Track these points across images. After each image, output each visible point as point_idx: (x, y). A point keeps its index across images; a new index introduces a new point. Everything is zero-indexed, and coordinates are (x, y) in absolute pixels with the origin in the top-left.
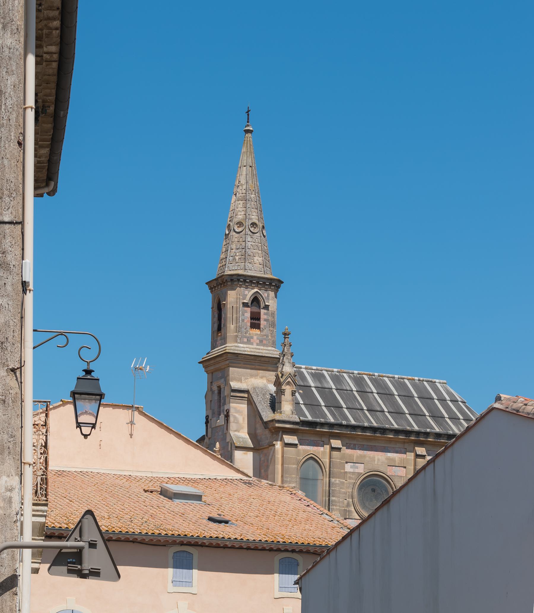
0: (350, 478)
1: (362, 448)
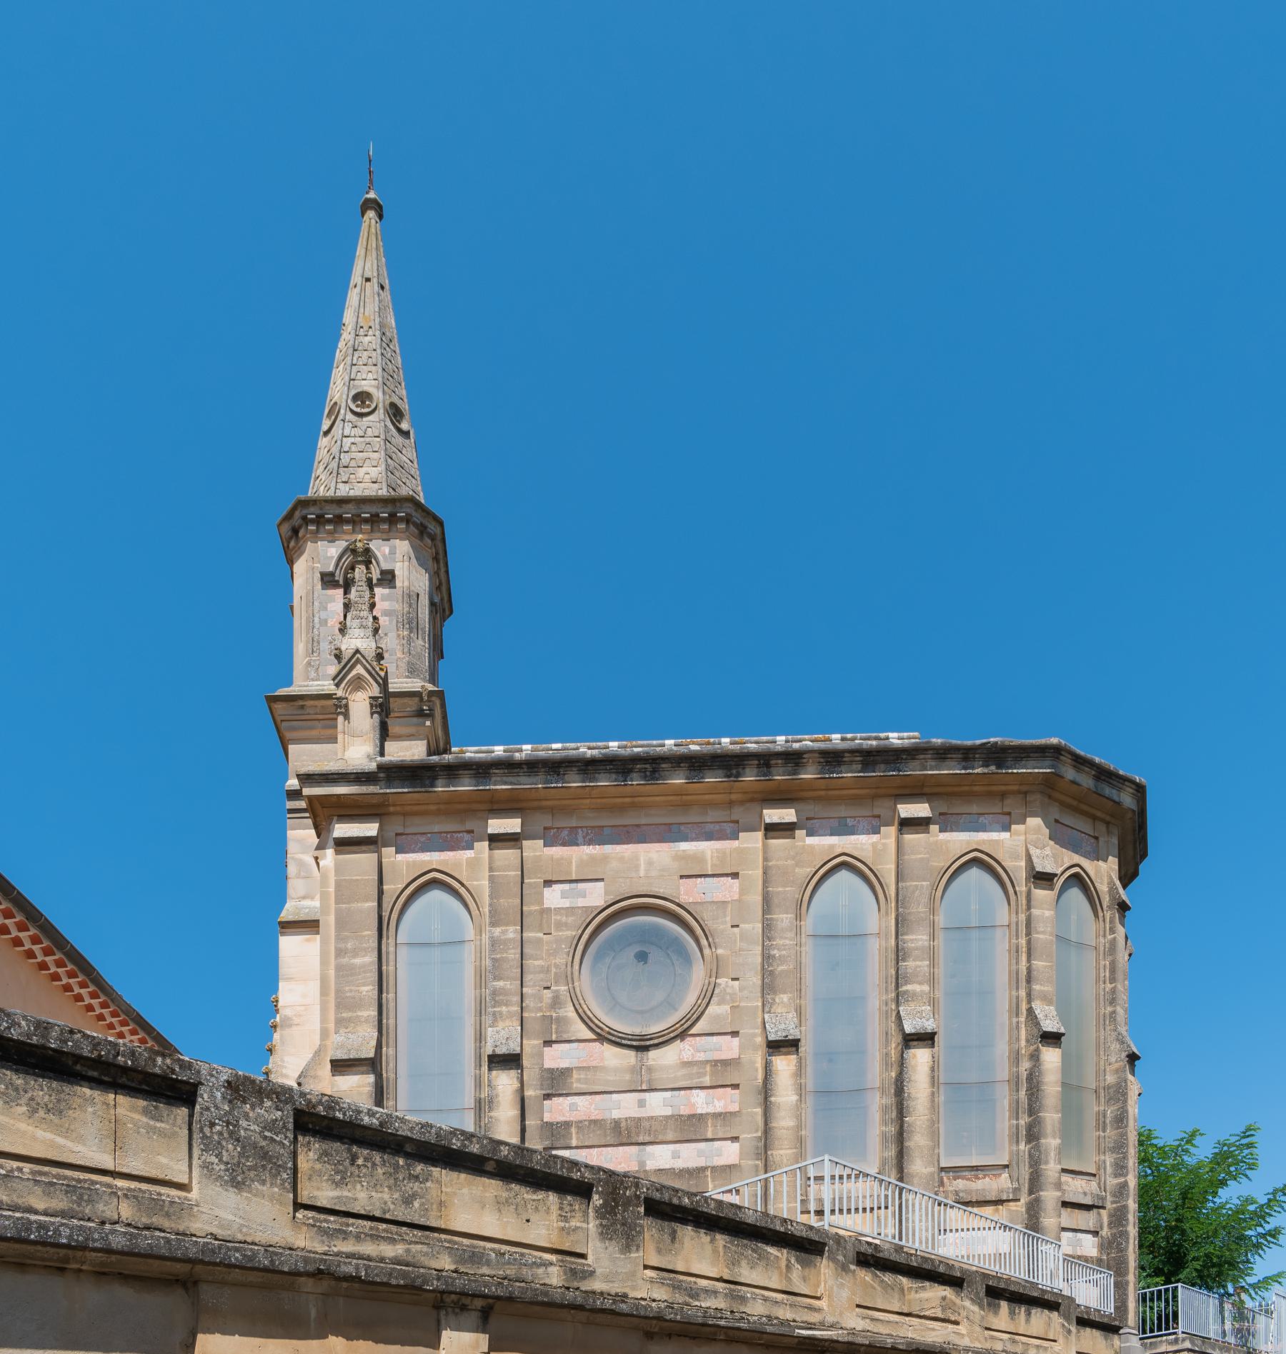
0: (559, 925)
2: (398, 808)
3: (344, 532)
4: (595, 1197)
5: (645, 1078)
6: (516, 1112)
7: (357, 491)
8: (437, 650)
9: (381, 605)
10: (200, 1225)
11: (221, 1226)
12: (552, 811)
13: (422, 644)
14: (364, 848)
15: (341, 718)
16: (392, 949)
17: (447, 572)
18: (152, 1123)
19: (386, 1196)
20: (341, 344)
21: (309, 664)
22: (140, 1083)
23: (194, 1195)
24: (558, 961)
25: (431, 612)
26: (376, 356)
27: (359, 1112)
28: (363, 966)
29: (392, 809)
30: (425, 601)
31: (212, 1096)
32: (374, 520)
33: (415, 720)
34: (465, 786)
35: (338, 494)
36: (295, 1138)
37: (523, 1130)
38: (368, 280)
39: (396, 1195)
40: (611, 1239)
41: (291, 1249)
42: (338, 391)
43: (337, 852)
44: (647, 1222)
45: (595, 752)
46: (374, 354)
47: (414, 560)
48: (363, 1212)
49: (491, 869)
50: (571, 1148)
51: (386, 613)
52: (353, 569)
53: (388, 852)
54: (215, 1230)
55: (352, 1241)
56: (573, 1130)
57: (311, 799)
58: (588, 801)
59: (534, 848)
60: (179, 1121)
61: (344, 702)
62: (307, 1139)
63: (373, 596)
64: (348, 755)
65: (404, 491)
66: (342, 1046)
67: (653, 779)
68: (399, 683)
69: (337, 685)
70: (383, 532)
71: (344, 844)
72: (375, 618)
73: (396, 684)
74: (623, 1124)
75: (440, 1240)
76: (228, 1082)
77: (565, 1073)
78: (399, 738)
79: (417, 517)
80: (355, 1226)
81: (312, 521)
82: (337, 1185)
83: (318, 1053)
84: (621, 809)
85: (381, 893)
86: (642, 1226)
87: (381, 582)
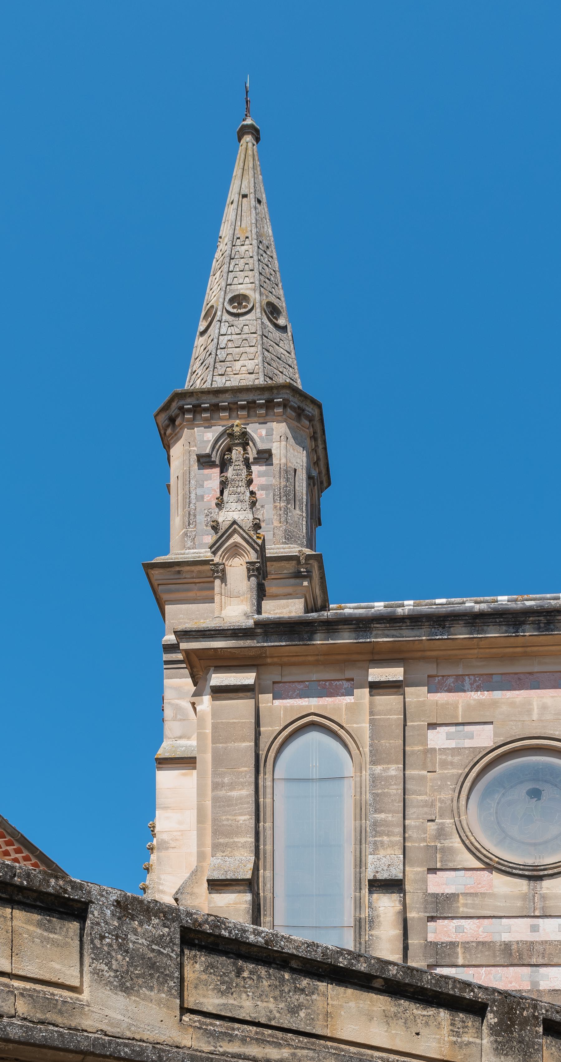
0: (444, 764)
1: (487, 683)
2: (276, 660)
3: (220, 419)
4: (490, 1016)
5: (539, 905)
6: (397, 932)
7: (234, 382)
8: (315, 517)
9: (258, 481)
10: (91, 1022)
11: (111, 1024)
12: (437, 660)
13: (299, 514)
14: (241, 695)
15: (217, 582)
16: (269, 783)
17: (325, 449)
18: (46, 934)
19: (272, 1006)
20: (218, 255)
21: (186, 534)
22: (35, 900)
23: (85, 996)
24: (443, 796)
25: (308, 485)
26: (253, 262)
27: (245, 931)
28: (241, 798)
29: (269, 660)
30: (302, 476)
31: (102, 913)
32: (251, 406)
33: (292, 581)
34: (345, 639)
35: (215, 385)
36: (182, 952)
37: (406, 948)
38: (245, 196)
39: (282, 1005)
40: (506, 1055)
41: (177, 1047)
42: (215, 294)
43: (214, 699)
44: (545, 1041)
45: (483, 606)
46: (251, 261)
47: (291, 440)
48: (248, 1018)
49: (371, 713)
50: (457, 966)
51: (263, 488)
52: (230, 450)
53: (266, 699)
54: (105, 1028)
55: (237, 1043)
56: (460, 950)
57: (187, 652)
58: (476, 651)
59: (417, 695)
60: (71, 933)
61: (221, 567)
62: (193, 953)
63: (250, 473)
64: (224, 614)
65: (281, 379)
66: (219, 868)
67: (547, 630)
68: (274, 549)
69: (214, 553)
70: (260, 416)
71: (220, 692)
72: (252, 493)
73: (273, 550)
74: (514, 947)
75: (326, 1047)
76: (117, 901)
77: (451, 898)
78: (275, 597)
79: (295, 401)
80: (239, 1030)
81: (189, 411)
82: (223, 993)
83: (194, 873)
84: (512, 658)
85: (258, 734)
86: (541, 1045)
87: (257, 461)
